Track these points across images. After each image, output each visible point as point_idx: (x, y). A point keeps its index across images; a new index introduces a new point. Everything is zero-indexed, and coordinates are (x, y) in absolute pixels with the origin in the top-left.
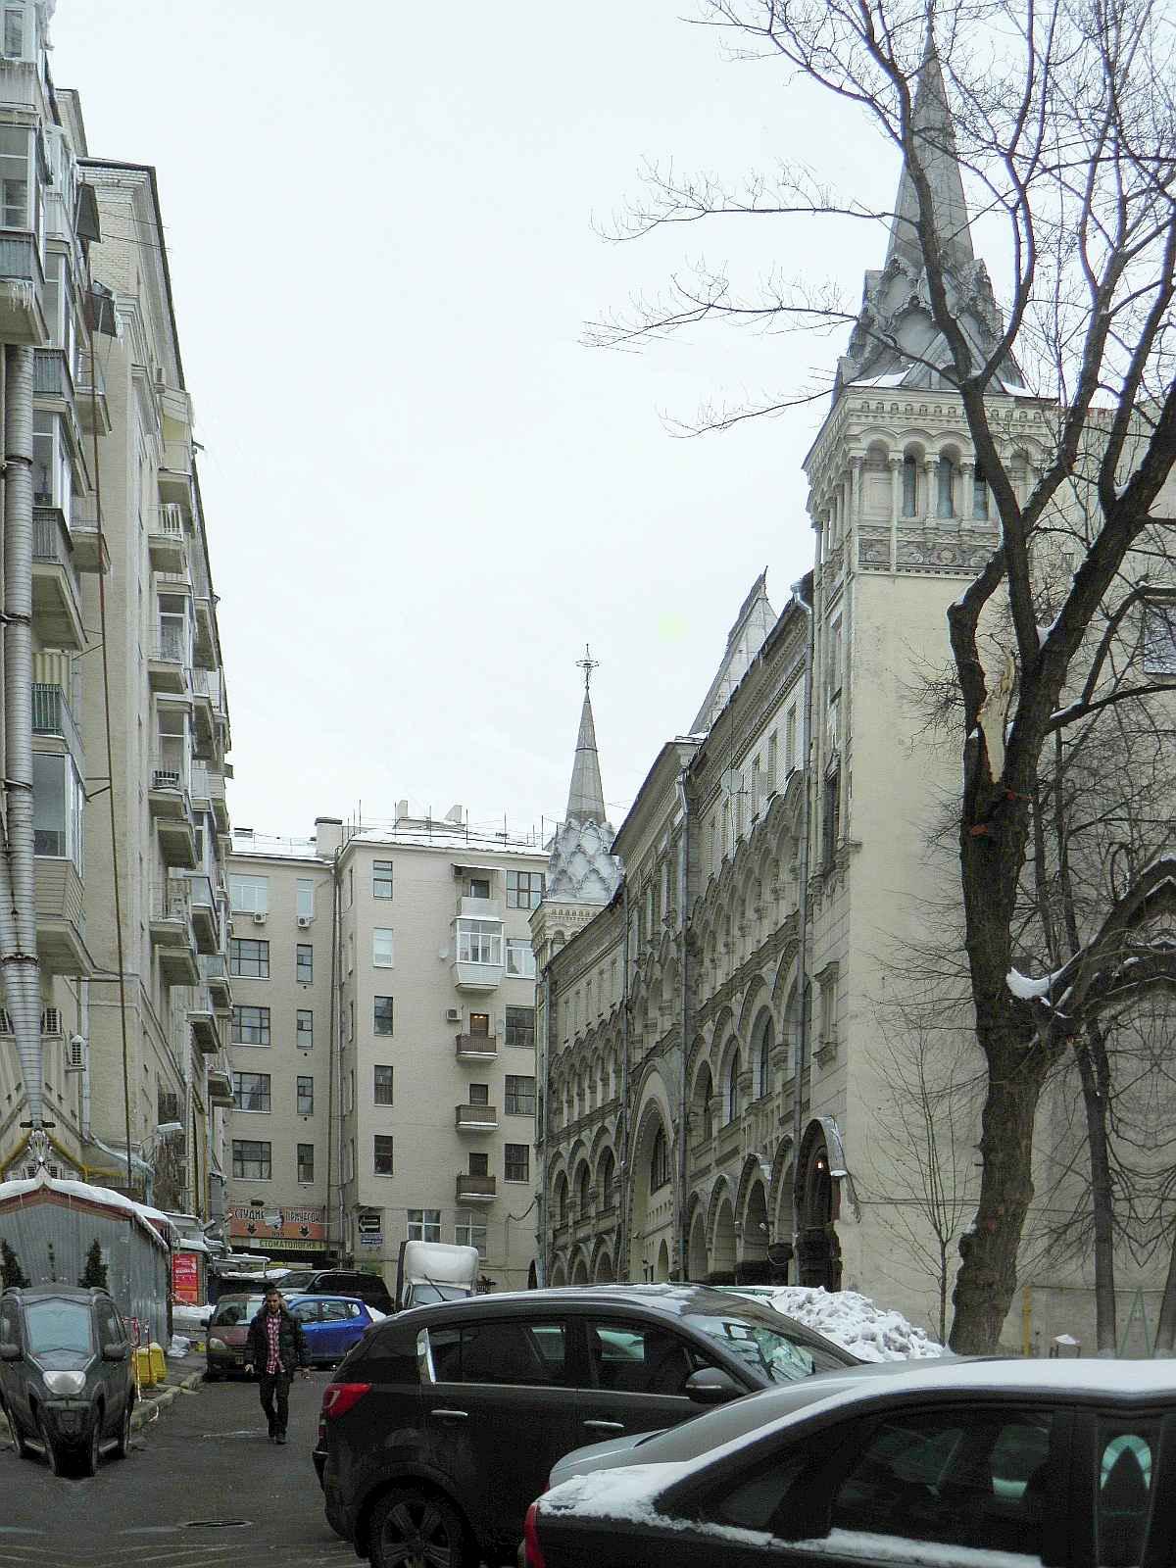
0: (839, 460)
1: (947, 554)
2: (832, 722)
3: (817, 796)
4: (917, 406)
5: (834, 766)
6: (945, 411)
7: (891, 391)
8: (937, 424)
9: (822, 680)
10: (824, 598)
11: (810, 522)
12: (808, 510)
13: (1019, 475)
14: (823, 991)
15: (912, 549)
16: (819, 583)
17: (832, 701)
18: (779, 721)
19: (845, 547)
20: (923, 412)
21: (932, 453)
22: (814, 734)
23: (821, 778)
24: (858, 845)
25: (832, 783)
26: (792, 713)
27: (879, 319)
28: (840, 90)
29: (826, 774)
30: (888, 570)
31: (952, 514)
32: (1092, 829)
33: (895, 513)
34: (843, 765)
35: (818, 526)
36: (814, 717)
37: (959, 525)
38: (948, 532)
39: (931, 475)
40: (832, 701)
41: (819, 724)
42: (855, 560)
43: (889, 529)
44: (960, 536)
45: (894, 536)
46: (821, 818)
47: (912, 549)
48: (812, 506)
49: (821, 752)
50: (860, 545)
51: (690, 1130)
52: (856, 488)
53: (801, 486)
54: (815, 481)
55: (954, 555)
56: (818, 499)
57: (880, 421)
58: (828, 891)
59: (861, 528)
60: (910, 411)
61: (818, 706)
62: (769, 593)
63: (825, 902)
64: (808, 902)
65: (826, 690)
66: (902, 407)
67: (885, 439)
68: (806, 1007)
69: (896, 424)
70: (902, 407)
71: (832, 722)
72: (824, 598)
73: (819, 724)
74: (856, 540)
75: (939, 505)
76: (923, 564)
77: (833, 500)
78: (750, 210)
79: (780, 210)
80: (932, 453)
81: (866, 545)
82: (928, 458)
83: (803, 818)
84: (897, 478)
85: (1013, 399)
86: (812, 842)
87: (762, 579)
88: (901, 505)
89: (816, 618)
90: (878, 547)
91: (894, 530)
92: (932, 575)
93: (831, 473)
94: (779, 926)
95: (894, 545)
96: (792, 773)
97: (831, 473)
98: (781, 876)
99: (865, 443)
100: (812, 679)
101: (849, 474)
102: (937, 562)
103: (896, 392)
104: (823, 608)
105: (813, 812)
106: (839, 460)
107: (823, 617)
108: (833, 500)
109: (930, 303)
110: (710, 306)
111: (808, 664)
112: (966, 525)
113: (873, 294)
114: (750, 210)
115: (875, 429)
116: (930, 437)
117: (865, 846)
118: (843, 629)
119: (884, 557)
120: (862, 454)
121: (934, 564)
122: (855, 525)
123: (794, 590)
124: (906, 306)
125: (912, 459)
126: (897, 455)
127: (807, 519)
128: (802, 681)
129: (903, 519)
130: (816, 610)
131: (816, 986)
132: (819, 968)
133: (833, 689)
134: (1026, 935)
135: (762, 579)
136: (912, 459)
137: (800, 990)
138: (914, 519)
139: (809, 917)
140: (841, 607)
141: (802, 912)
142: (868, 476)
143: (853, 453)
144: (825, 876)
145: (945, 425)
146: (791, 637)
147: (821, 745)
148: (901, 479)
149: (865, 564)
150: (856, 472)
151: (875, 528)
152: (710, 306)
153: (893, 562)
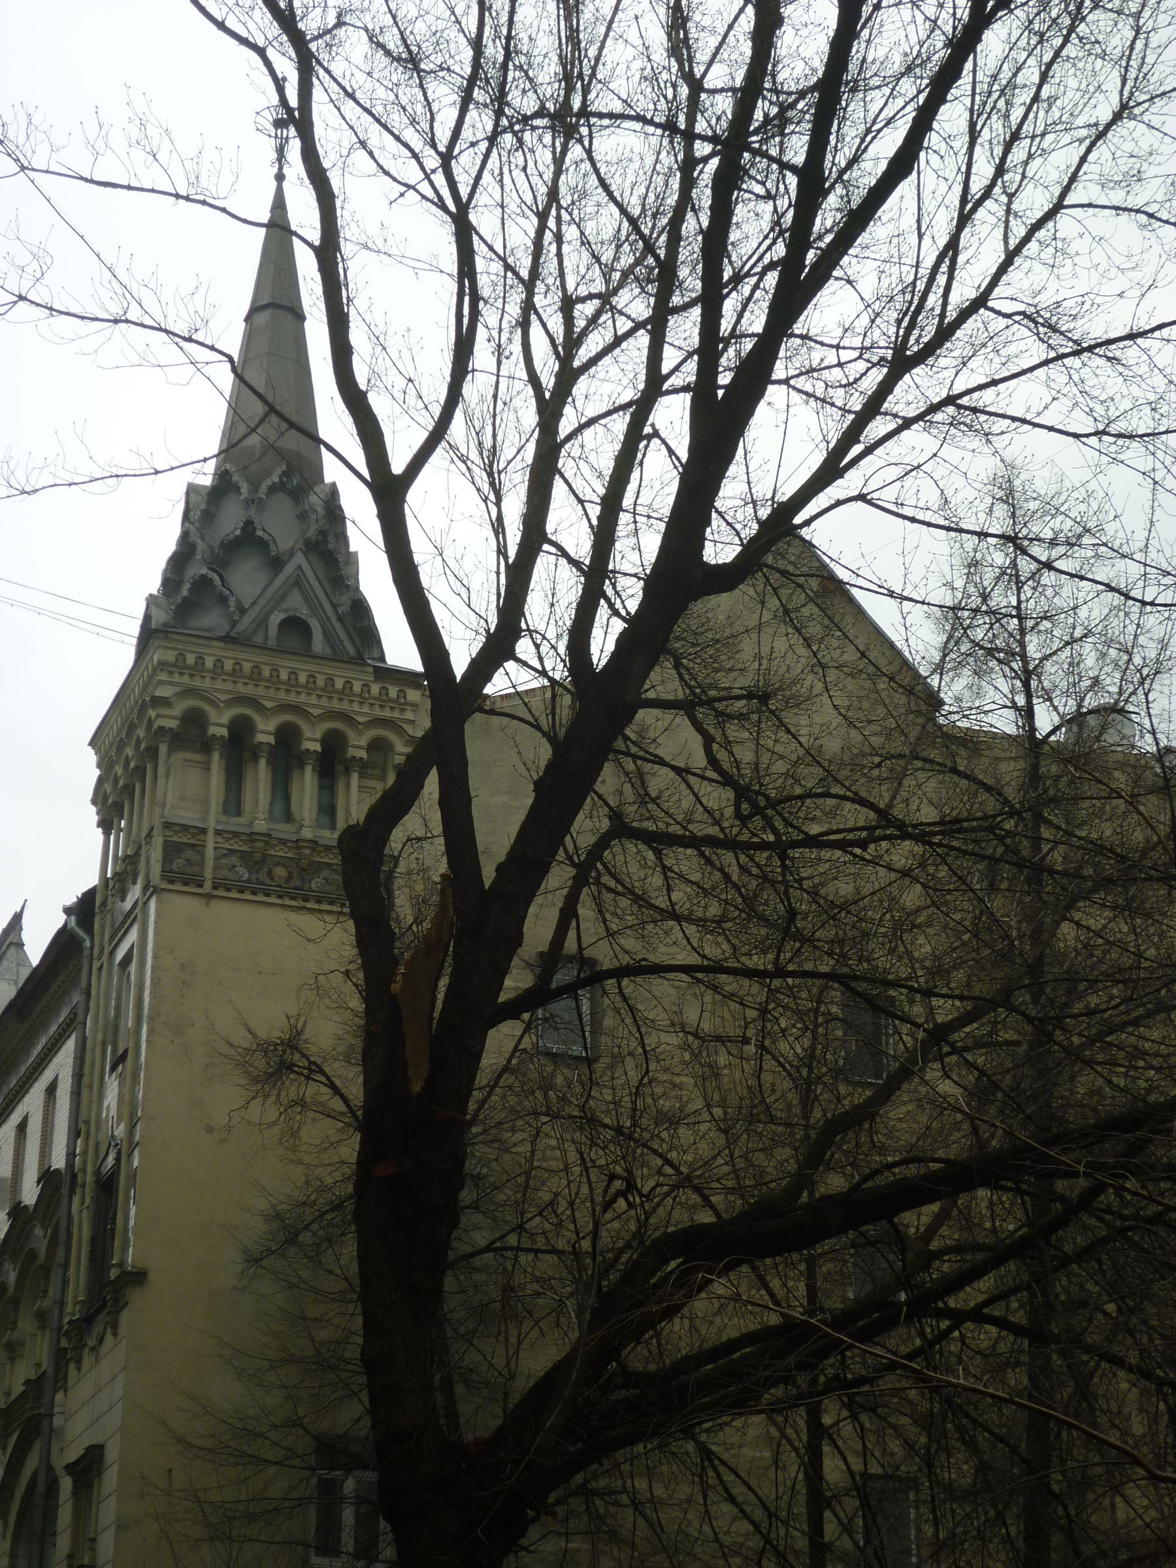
0: (141, 732)
1: (280, 872)
2: (111, 1097)
3: (80, 1209)
4: (247, 667)
5: (110, 1161)
6: (284, 676)
7: (215, 643)
8: (271, 693)
9: (100, 1038)
10: (108, 924)
11: (96, 818)
12: (94, 802)
13: (375, 772)
14: (75, 1493)
15: (234, 860)
16: (104, 904)
17: (113, 1069)
18: (33, 1102)
19: (143, 852)
20: (255, 677)
21: (265, 731)
22: (83, 1115)
23: (90, 1179)
24: (138, 1277)
25: (107, 1187)
26: (51, 1090)
27: (201, 546)
28: (221, 26)
29: (97, 1172)
30: (201, 886)
31: (288, 817)
32: (479, 1261)
33: (213, 808)
34: (124, 1158)
35: (106, 824)
36: (85, 1092)
37: (297, 833)
38: (283, 842)
39: (263, 763)
40: (113, 1069)
41: (90, 1101)
42: (156, 869)
43: (203, 831)
44: (299, 848)
45: (210, 840)
46: (86, 1234)
47: (234, 860)
48: (99, 798)
49: (92, 1143)
50: (165, 850)
51: (583, 243)
52: (161, 770)
53: (87, 770)
54: (105, 764)
55: (290, 874)
56: (108, 788)
57: (197, 682)
58: (91, 1342)
59: (167, 825)
60: (236, 673)
61: (92, 1075)
62: (25, 936)
63: (87, 1361)
64: (61, 1359)
65: (104, 1052)
66: (228, 665)
67: (206, 707)
68: (50, 1513)
69: (222, 688)
70: (228, 665)
71: (111, 1097)
72: (108, 924)
73: (90, 1101)
74: (158, 841)
75: (271, 804)
76: (248, 881)
77: (129, 790)
78: (86, 180)
79: (129, 188)
80: (265, 731)
81: (171, 851)
82: (260, 738)
83: (60, 1240)
84: (216, 761)
85: (371, 669)
86: (72, 1272)
87: (17, 920)
88: (222, 799)
89: (96, 952)
90: (189, 854)
91: (211, 834)
92: (260, 898)
93: (129, 751)
94: (13, 1397)
95: (210, 853)
96: (48, 1177)
97: (129, 751)
98: (20, 1324)
99: (178, 709)
100: (84, 1039)
101: (153, 752)
102: (268, 881)
103: (222, 645)
104: (107, 938)
105: (75, 1229)
106: (141, 732)
107: (106, 952)
108: (129, 790)
109: (260, 547)
110: (22, 298)
111: (80, 1018)
112: (307, 833)
113: (196, 515)
114: (86, 180)
115: (190, 692)
116: (261, 709)
117: (152, 1276)
118: (133, 968)
119: (196, 869)
120: (173, 724)
121: (263, 883)
122: (157, 822)
123: (68, 911)
124: (238, 532)
125: (241, 731)
126: (218, 729)
127: (91, 815)
128: (70, 1045)
129: (224, 818)
130: (96, 941)
131: (66, 1484)
132: (73, 1454)
133: (114, 1051)
134: (797, 981)
135: (17, 920)
136: (241, 731)
137: (41, 1488)
138: (241, 820)
139: (60, 1380)
140: (133, 936)
141: (50, 1373)
142: (179, 756)
143: (161, 722)
144: (88, 1320)
145: (282, 695)
146: (58, 982)
147: (93, 1131)
148: (223, 764)
149: (169, 876)
150: (163, 749)
151: (185, 828)
152: (22, 298)
153: (208, 873)
